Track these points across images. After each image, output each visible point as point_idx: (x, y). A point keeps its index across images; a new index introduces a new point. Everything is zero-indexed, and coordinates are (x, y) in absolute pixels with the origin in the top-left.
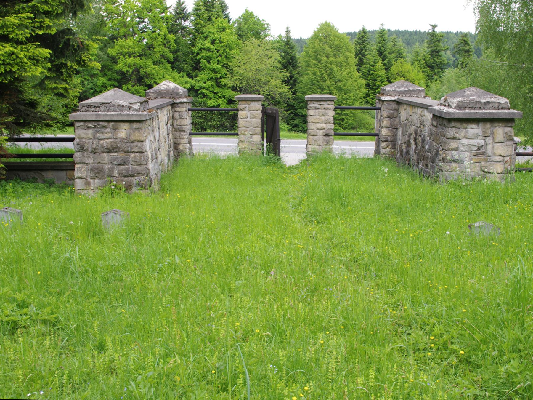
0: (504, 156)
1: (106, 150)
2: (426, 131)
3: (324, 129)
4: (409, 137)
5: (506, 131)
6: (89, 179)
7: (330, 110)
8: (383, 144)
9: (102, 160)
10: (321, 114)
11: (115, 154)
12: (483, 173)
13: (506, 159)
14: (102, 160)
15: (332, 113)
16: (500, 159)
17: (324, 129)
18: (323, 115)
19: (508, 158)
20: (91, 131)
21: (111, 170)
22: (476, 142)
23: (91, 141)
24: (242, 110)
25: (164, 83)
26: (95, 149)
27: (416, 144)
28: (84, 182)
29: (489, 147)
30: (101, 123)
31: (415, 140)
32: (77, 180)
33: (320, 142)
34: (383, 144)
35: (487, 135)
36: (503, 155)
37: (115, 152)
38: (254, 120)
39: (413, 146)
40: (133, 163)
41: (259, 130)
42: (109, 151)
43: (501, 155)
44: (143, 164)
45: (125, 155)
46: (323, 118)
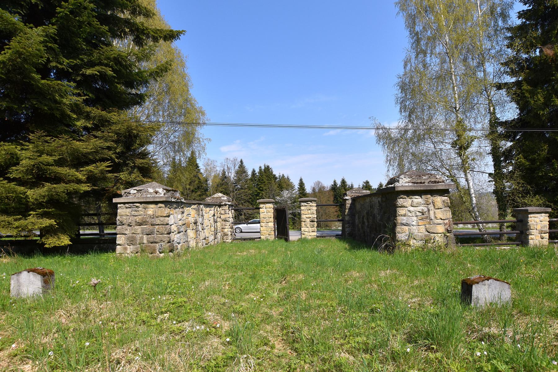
0: (444, 220)
1: (138, 224)
2: (376, 211)
3: (310, 218)
4: (363, 218)
5: (443, 200)
6: (127, 246)
7: (314, 206)
8: (347, 226)
9: (135, 231)
10: (308, 209)
11: (145, 226)
12: (427, 233)
13: (447, 221)
14: (135, 231)
15: (315, 208)
16: (441, 222)
17: (310, 218)
18: (310, 210)
19: (447, 221)
20: (128, 210)
21: (142, 238)
22: (420, 209)
23: (128, 217)
24: (261, 208)
25: (217, 194)
26: (130, 223)
27: (368, 222)
28: (122, 248)
29: (432, 213)
30: (135, 204)
31: (368, 219)
32: (118, 247)
33: (308, 225)
34: (347, 226)
35: (428, 203)
36: (442, 218)
37: (145, 225)
38: (269, 213)
39: (366, 224)
40: (157, 233)
41: (272, 219)
42: (140, 224)
43: (441, 219)
44: (164, 233)
45: (151, 227)
46: (309, 211)
